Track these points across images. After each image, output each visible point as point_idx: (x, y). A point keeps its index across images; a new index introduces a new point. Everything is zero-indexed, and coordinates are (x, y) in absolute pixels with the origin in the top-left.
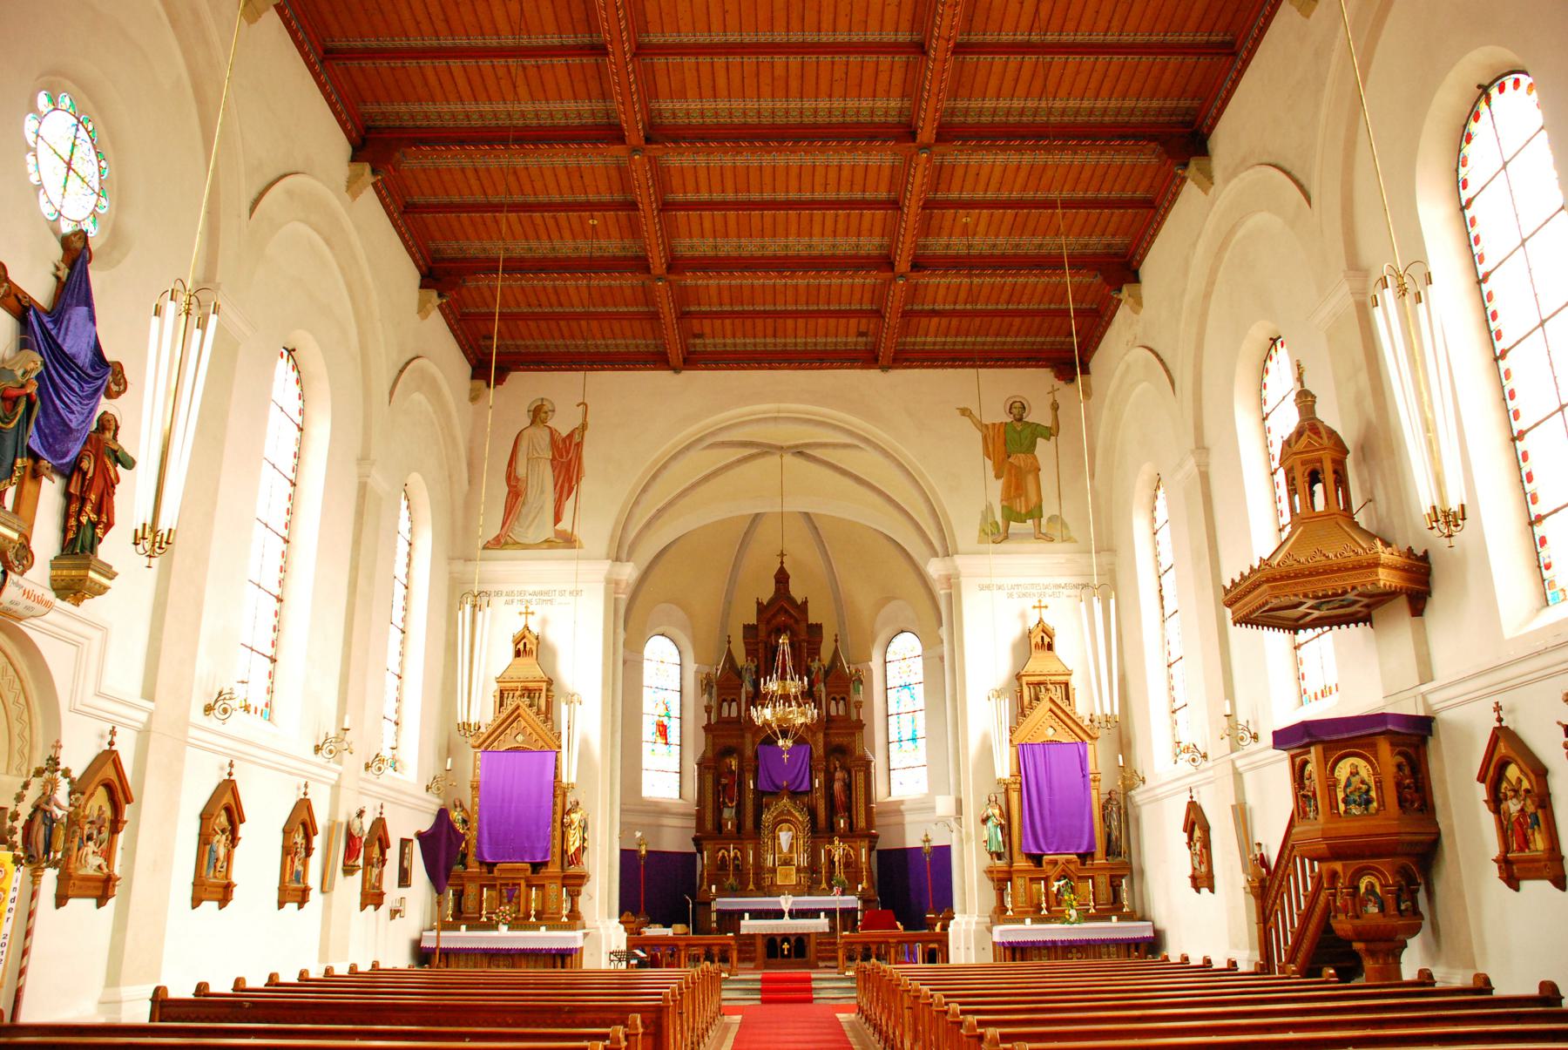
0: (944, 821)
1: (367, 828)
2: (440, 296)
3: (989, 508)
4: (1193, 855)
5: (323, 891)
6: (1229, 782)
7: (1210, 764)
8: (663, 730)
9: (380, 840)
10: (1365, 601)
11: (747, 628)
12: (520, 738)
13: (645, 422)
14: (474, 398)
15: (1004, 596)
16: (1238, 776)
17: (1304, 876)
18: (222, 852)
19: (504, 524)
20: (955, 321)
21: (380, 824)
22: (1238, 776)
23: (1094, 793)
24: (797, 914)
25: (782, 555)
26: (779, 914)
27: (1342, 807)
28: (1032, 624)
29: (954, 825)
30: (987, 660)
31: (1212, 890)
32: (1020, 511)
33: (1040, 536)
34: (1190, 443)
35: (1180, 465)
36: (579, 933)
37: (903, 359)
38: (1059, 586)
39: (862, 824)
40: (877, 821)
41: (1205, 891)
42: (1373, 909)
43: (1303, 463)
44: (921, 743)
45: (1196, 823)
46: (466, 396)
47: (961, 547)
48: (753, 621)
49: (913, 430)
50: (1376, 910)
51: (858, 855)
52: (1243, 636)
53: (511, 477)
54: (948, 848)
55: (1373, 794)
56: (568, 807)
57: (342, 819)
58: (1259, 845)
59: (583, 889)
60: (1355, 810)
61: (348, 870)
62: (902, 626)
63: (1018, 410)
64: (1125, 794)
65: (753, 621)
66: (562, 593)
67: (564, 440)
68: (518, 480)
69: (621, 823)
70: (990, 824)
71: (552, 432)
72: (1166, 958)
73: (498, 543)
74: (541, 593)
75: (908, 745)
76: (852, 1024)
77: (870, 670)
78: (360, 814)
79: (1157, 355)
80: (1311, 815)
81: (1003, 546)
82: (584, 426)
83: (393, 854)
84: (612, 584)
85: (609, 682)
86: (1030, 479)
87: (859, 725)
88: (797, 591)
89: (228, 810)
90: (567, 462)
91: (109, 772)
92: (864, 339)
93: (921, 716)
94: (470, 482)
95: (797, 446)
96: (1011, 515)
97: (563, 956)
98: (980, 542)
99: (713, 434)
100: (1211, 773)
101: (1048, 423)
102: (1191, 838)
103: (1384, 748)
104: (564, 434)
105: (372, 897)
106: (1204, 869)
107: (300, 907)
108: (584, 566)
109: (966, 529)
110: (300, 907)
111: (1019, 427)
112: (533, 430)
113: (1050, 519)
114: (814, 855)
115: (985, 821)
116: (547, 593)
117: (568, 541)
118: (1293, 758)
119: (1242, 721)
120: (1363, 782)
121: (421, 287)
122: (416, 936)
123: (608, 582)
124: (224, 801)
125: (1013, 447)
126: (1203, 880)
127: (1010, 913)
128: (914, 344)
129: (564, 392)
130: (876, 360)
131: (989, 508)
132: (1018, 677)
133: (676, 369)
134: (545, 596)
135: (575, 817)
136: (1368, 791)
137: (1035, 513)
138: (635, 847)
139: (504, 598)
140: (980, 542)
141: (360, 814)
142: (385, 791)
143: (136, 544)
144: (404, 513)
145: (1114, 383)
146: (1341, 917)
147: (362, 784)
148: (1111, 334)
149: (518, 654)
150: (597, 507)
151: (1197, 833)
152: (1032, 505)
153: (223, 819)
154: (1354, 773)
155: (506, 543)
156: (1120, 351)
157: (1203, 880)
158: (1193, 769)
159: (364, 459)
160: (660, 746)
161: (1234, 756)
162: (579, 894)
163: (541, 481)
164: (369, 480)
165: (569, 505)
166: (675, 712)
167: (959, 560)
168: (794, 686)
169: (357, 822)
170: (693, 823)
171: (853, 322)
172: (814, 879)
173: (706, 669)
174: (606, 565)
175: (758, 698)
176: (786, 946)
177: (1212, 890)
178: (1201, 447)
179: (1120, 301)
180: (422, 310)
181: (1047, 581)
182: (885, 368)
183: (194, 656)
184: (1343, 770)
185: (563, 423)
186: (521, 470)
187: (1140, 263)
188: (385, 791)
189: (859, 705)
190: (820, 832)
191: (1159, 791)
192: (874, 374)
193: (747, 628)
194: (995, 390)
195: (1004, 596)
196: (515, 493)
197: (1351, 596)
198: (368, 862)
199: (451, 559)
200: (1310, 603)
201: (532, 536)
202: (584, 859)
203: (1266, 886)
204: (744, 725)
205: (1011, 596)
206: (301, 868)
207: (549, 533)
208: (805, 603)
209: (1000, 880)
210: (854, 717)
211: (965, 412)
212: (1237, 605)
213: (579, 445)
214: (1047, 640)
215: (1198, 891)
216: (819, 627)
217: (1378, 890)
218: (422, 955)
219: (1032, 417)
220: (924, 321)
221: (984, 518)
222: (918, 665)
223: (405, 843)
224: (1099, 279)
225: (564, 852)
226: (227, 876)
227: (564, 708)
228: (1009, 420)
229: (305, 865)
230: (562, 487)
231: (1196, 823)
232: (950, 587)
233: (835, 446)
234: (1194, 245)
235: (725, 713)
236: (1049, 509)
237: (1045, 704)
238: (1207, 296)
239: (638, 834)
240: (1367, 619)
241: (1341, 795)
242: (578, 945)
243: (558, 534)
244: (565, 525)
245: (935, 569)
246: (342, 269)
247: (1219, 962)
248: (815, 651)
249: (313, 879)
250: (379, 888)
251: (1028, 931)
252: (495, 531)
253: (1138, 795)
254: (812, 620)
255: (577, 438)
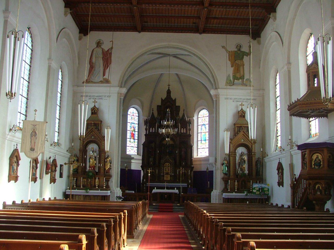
0: (211, 164)
1: (51, 162)
2: (70, 10)
3: (229, 76)
4: (279, 176)
5: (40, 178)
6: (289, 157)
7: (285, 152)
8: (133, 135)
9: (55, 165)
10: (326, 111)
11: (158, 106)
12: (93, 137)
13: (130, 46)
14: (80, 39)
15: (231, 101)
16: (291, 156)
17: (304, 183)
18: (15, 168)
19: (88, 77)
20: (222, 21)
21: (55, 161)
22: (291, 156)
23: (254, 158)
24: (168, 188)
25: (169, 85)
26: (163, 188)
27: (313, 166)
28: (240, 109)
29: (214, 165)
30: (226, 118)
31: (283, 186)
32: (238, 78)
33: (243, 84)
34: (286, 62)
35: (283, 68)
36: (109, 191)
37: (206, 31)
38: (248, 99)
39: (189, 163)
40: (194, 163)
41: (281, 186)
42: (319, 193)
43: (312, 72)
44: (207, 141)
45: (280, 168)
46: (78, 38)
47: (220, 87)
48: (160, 104)
49: (210, 51)
50: (319, 193)
51: (188, 172)
52: (295, 119)
53: (91, 62)
54: (213, 171)
55: (322, 163)
56: (106, 157)
57: (45, 159)
58: (295, 175)
59: (110, 180)
60: (316, 167)
61: (47, 173)
62: (203, 107)
63: (239, 47)
64: (262, 159)
65: (160, 104)
66: (105, 96)
67: (106, 52)
68: (92, 63)
69: (121, 161)
70: (224, 165)
71: (103, 49)
72: (272, 204)
73: (88, 81)
74: (99, 96)
75: (203, 142)
76: (183, 218)
77: (194, 120)
78: (50, 158)
79: (279, 35)
80: (305, 168)
81: (233, 87)
82: (112, 48)
83: (58, 169)
84: (119, 94)
85: (118, 122)
86: (241, 68)
87: (190, 136)
88: (173, 96)
89: (16, 157)
90: (107, 58)
91: (16, 154)
92: (195, 25)
93: (207, 134)
94: (79, 64)
95: (174, 55)
96: (235, 78)
97: (105, 198)
98: (226, 85)
99: (150, 51)
100: (285, 154)
101: (248, 51)
102: (278, 172)
103: (326, 151)
104: (106, 50)
105: (53, 180)
106: (281, 180)
107: (35, 183)
108: (112, 89)
109: (222, 81)
110: (35, 183)
111: (239, 52)
112: (97, 49)
113: (246, 80)
114: (175, 172)
115: (223, 164)
116: (101, 96)
117: (107, 81)
118: (302, 153)
119: (294, 141)
120: (319, 160)
121: (65, 7)
122: (64, 191)
123: (118, 93)
124: (16, 155)
125: (237, 57)
126: (281, 183)
127: (236, 190)
128: (209, 26)
129: (107, 38)
130: (198, 31)
131: (229, 76)
132: (235, 124)
133: (139, 32)
134: (100, 97)
135: (108, 160)
136: (321, 162)
137: (242, 77)
138: (125, 168)
139: (88, 98)
140: (226, 85)
141: (50, 158)
142: (56, 152)
143: (7, 96)
144: (60, 73)
145: (267, 41)
146: (310, 195)
147: (50, 150)
148: (267, 26)
149: (92, 113)
150: (116, 72)
151: (280, 171)
152: (241, 75)
153: (15, 159)
154: (317, 157)
155: (89, 82)
156: (269, 32)
157: (281, 183)
158: (280, 153)
159: (50, 59)
160: (132, 140)
161: (291, 150)
162: (109, 181)
163: (99, 63)
164: (51, 65)
165: (107, 71)
166: (137, 130)
167: (219, 90)
168: (171, 123)
169: (49, 160)
170: (141, 162)
171: (192, 20)
172: (175, 179)
173: (146, 118)
174: (117, 89)
175: (161, 126)
176: (166, 196)
177: (283, 186)
178: (289, 63)
179: (270, 17)
180: (66, 14)
181: (244, 97)
182: (200, 33)
183: (7, 116)
184: (314, 157)
185: (106, 47)
186: (94, 60)
187: (277, 6)
188: (56, 152)
189: (190, 130)
190: (176, 166)
191: (271, 158)
192: (197, 35)
193: (158, 106)
194: (233, 41)
195: (231, 101)
196: (92, 67)
197: (321, 110)
198: (52, 171)
199: (74, 86)
200: (311, 111)
201: (97, 79)
202: (110, 171)
203: (295, 186)
204: (157, 134)
205: (234, 101)
206: (35, 172)
207: (101, 79)
208: (175, 100)
209: (226, 181)
210: (188, 133)
211: (223, 47)
212: (291, 110)
213: (111, 54)
214: (243, 114)
215: (279, 187)
216: (179, 107)
217: (321, 188)
218: (66, 196)
219: (243, 50)
220: (212, 20)
221: (227, 79)
222: (207, 119)
223: (61, 166)
224: (264, 11)
225: (105, 169)
226: (17, 174)
227: (106, 130)
228: (236, 50)
229: (36, 171)
230: (105, 66)
231: (280, 168)
232: (216, 98)
233: (185, 55)
234: (292, 3)
235: (151, 131)
236: (246, 77)
237: (242, 133)
238: (294, 19)
239: (125, 165)
240: (326, 116)
241: (313, 163)
242: (109, 194)
243: (104, 79)
244: (106, 77)
245: (212, 92)
246: (43, 4)
247: (280, 205)
248: (178, 114)
249: (38, 175)
250: (55, 178)
251: (234, 195)
252: (86, 78)
253: (266, 159)
254: (177, 104)
255: (110, 51)
